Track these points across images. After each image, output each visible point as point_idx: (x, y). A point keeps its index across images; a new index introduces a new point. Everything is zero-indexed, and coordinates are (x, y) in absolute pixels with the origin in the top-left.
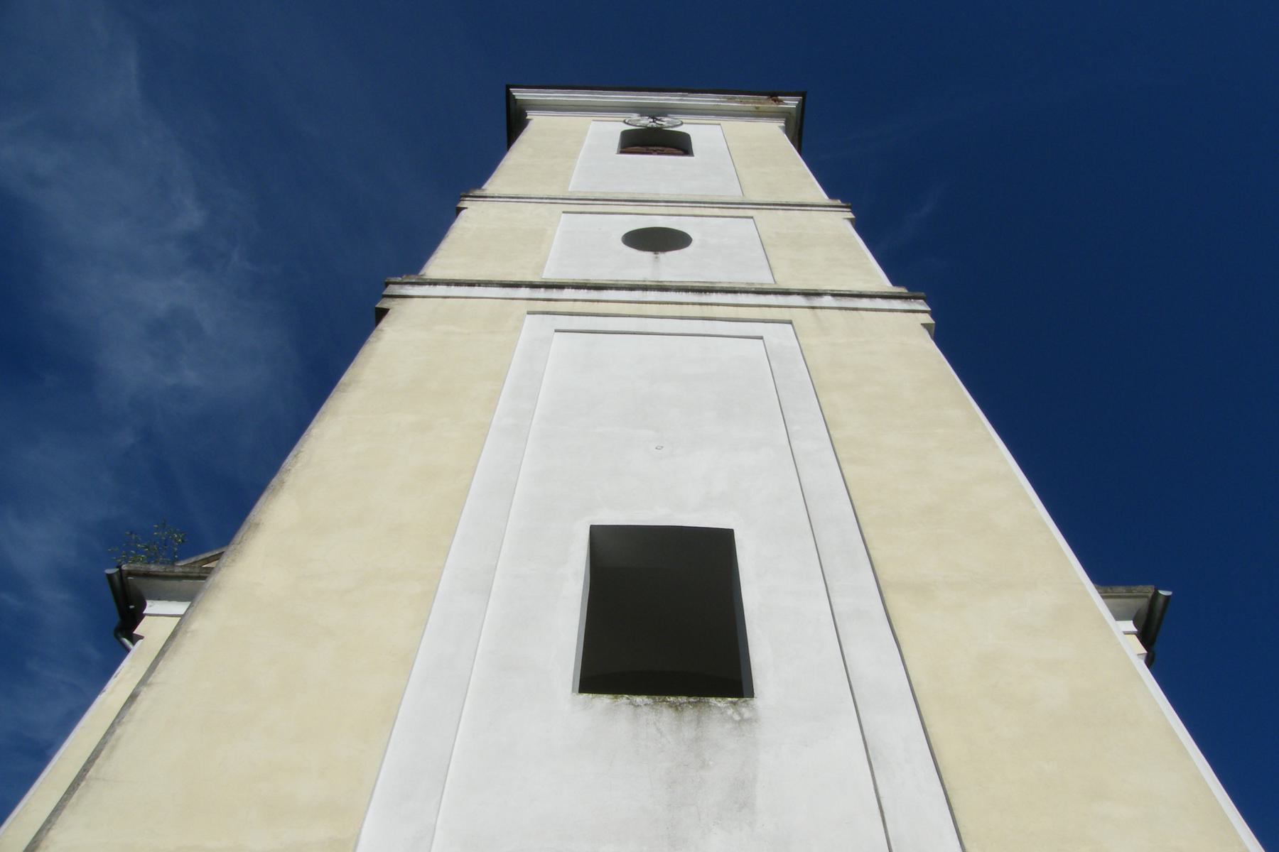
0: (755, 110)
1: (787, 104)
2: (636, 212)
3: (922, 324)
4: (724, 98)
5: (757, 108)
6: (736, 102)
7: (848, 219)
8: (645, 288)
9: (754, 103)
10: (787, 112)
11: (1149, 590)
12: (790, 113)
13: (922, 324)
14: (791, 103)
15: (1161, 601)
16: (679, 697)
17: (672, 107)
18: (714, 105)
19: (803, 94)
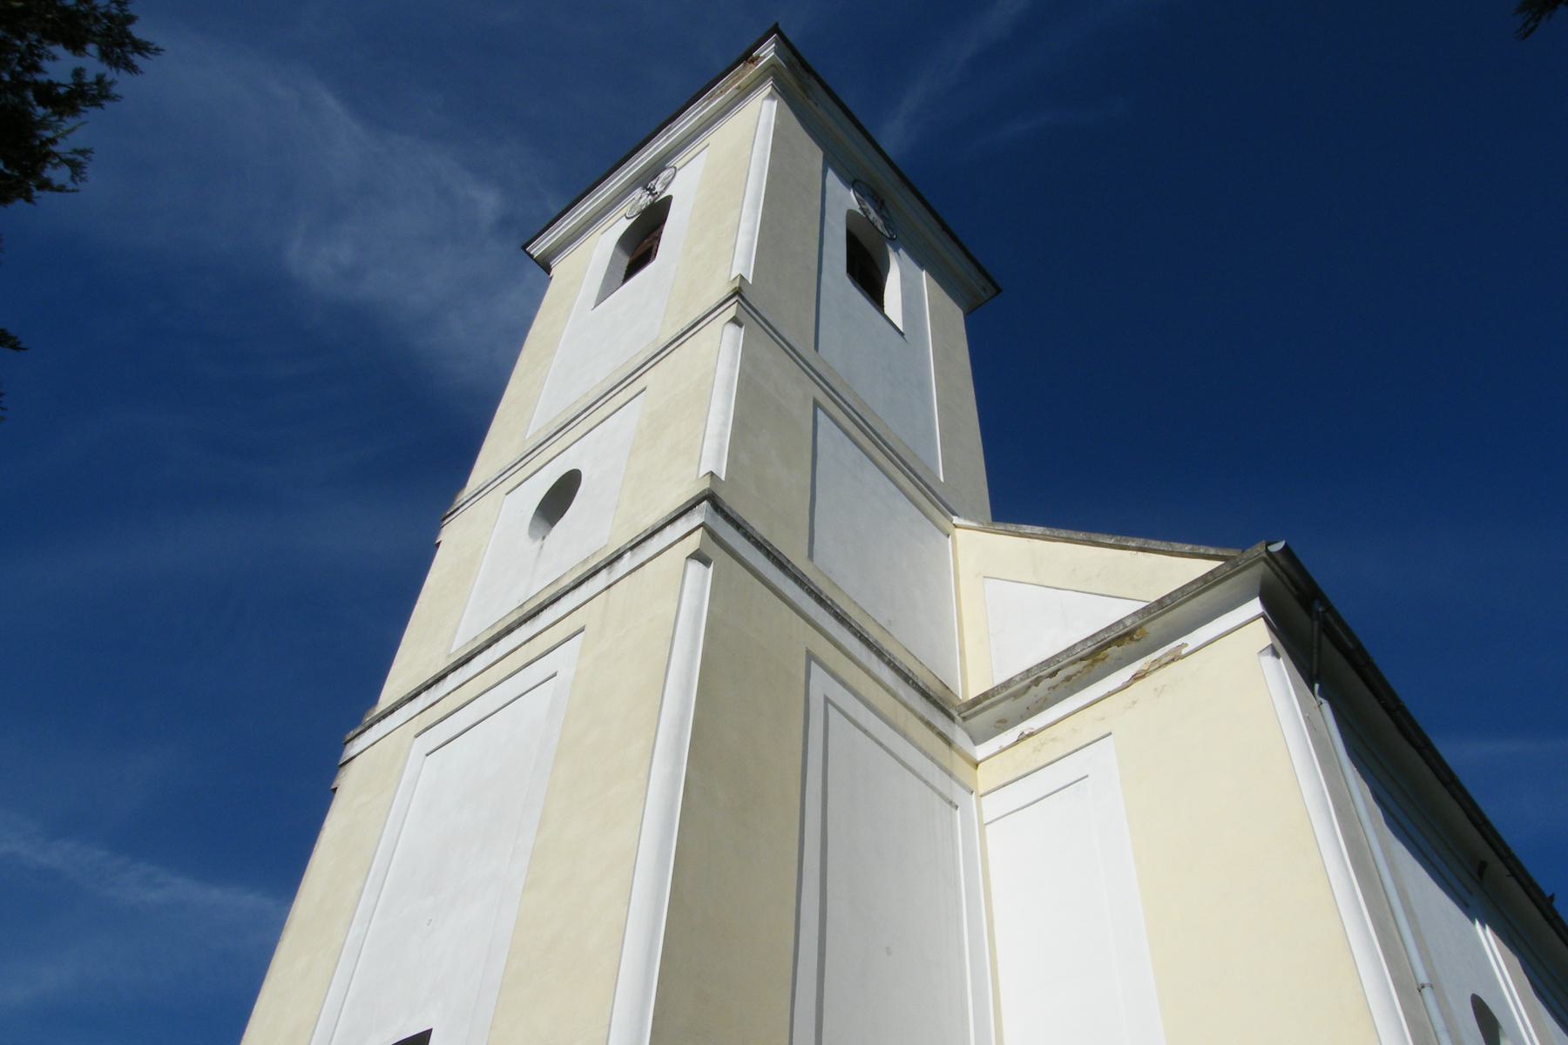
0: (738, 91)
1: (764, 57)
2: (529, 473)
3: (431, 1030)
4: (704, 100)
5: (739, 87)
6: (718, 96)
7: (729, 321)
8: (509, 630)
9: (734, 82)
10: (769, 67)
11: (1259, 549)
12: (773, 65)
13: (431, 1030)
14: (767, 52)
15: (1279, 557)
16: (1008, 525)
17: (670, 148)
18: (698, 119)
19: (775, 29)
